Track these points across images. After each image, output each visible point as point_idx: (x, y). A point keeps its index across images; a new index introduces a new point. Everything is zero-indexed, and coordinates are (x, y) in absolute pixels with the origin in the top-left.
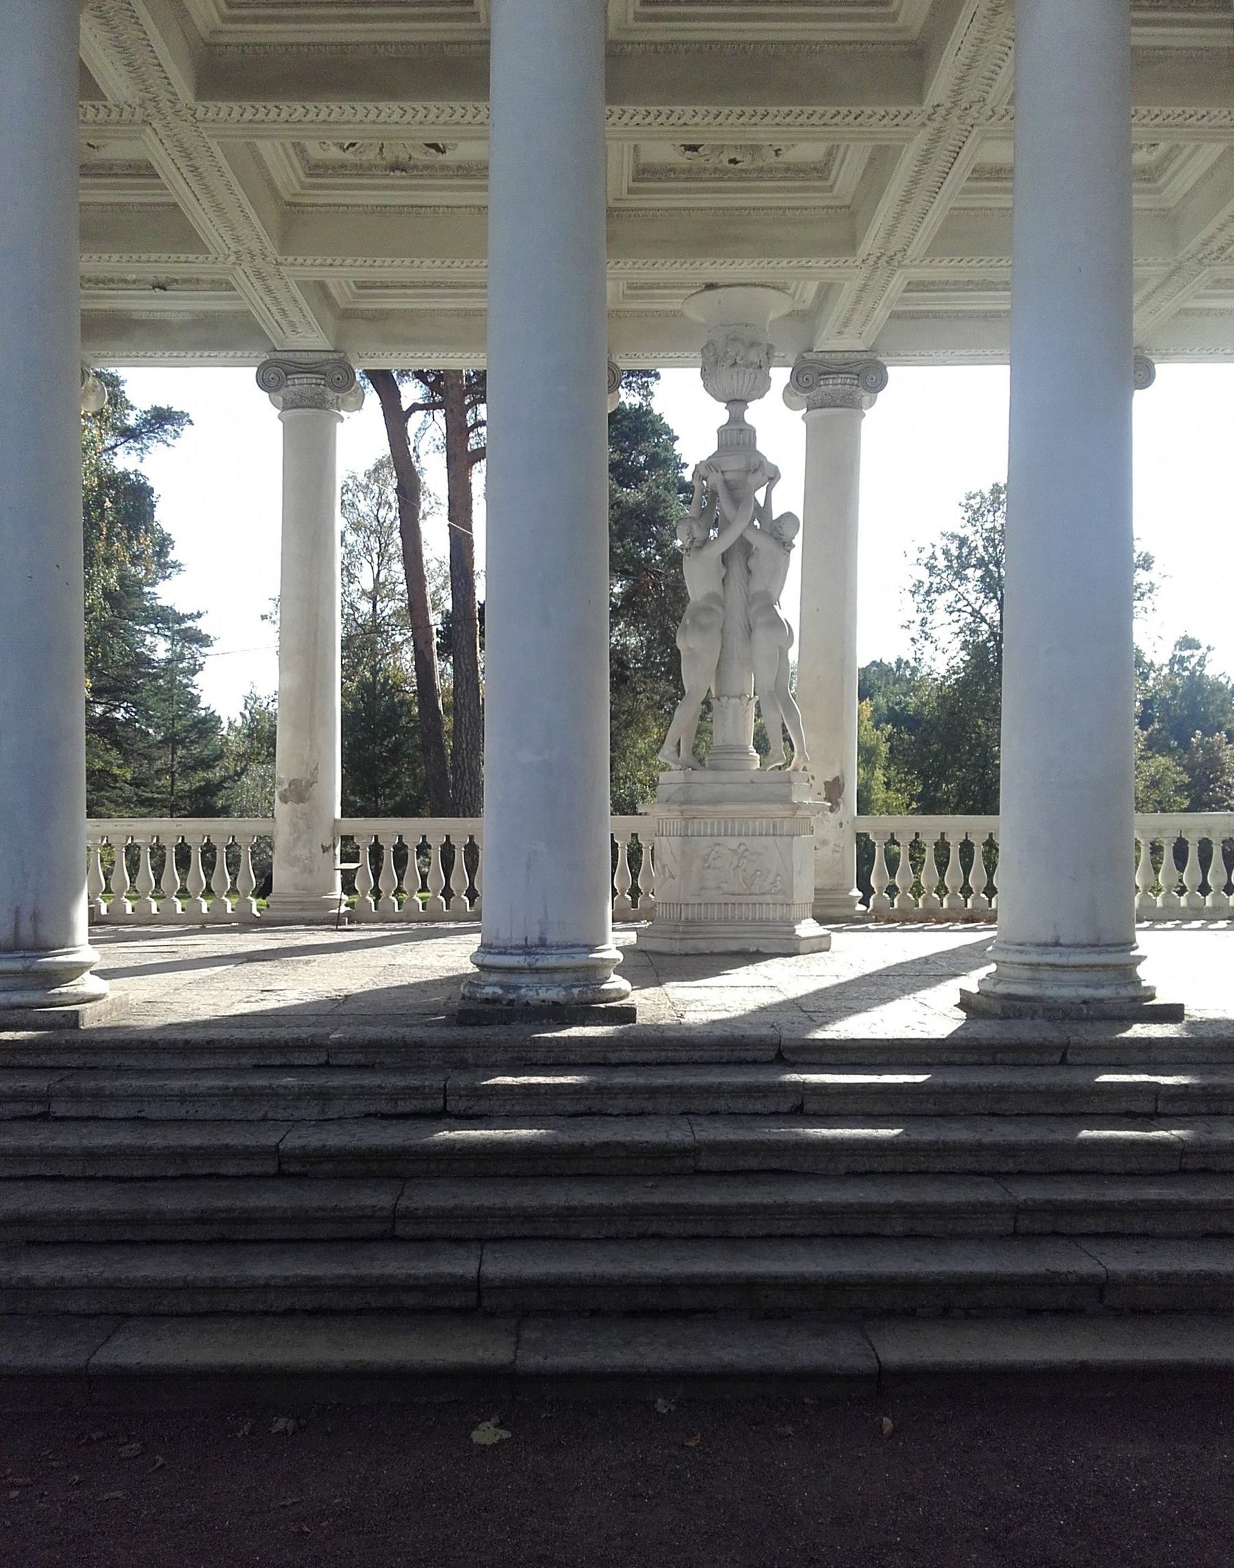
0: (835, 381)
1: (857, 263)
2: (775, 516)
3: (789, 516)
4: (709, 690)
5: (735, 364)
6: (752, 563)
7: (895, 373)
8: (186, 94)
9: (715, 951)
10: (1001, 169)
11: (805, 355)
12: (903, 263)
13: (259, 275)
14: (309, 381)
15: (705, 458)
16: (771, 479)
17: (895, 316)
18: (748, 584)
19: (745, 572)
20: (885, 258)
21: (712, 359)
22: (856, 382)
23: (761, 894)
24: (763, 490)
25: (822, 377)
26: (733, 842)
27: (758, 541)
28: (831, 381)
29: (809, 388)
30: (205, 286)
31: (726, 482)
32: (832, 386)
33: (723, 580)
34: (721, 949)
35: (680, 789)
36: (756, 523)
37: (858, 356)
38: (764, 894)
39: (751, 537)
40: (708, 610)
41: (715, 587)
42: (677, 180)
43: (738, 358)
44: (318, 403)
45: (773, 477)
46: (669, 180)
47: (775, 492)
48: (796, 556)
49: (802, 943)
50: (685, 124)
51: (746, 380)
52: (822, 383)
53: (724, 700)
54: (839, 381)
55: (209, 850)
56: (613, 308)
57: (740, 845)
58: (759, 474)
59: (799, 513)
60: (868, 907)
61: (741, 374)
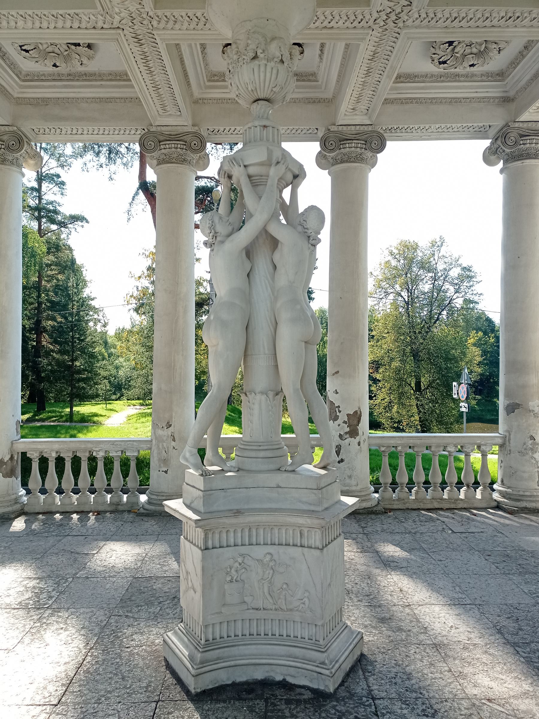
0: (350, 145)
2: (301, 210)
3: (313, 209)
5: (255, 57)
7: (389, 144)
11: (330, 127)
16: (295, 177)
19: (271, 268)
22: (364, 146)
23: (288, 610)
25: (342, 143)
26: (259, 552)
28: (347, 145)
32: (349, 149)
37: (366, 128)
38: (291, 610)
39: (273, 230)
43: (259, 51)
44: (359, 159)
47: (301, 190)
51: (268, 75)
52: (341, 146)
61: (262, 69)
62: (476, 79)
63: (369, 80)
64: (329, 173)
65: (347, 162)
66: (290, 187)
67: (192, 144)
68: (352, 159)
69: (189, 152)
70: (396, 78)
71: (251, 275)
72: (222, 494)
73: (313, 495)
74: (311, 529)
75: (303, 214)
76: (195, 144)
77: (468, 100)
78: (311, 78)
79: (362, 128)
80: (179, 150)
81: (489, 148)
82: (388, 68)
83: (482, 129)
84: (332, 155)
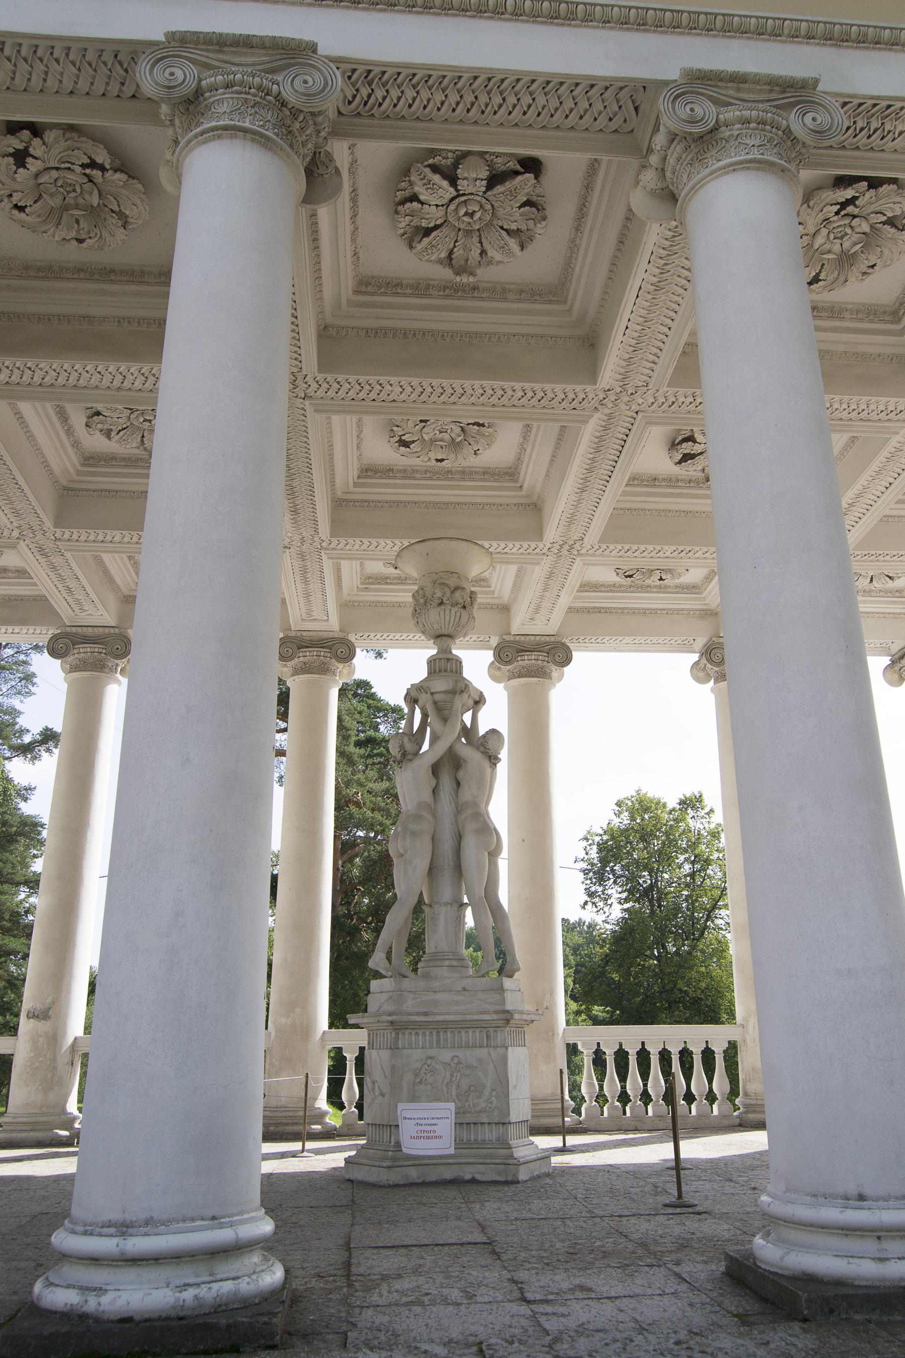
0: (530, 657)
1: (544, 551)
3: (493, 732)
4: (421, 894)
5: (441, 603)
6: (461, 774)
8: (48, 524)
9: (427, 1180)
10: (655, 479)
12: (582, 552)
13: (41, 549)
14: (92, 650)
15: (417, 682)
17: (570, 610)
18: (457, 796)
20: (566, 547)
21: (422, 601)
22: (547, 659)
24: (470, 713)
27: (466, 751)
28: (526, 657)
29: (508, 663)
30: (11, 575)
31: (435, 703)
32: (527, 660)
33: (433, 791)
34: (434, 1178)
35: (390, 998)
36: (463, 740)
37: (547, 639)
40: (418, 817)
41: (427, 796)
42: (394, 478)
43: (445, 599)
45: (479, 701)
46: (389, 478)
48: (502, 769)
49: (522, 1168)
50: (394, 400)
52: (519, 658)
53: (436, 907)
54: (533, 657)
55: (643, 1056)
56: (349, 599)
57: (452, 1058)
58: (465, 696)
59: (504, 729)
60: (580, 1116)
61: (448, 612)
62: (670, 590)
63: (547, 594)
64: (505, 688)
65: (526, 676)
66: (471, 712)
67: (339, 652)
68: (533, 673)
69: (333, 660)
70: (629, 481)
71: (436, 790)
72: (411, 995)
73: (498, 995)
74: (496, 1029)
75: (484, 736)
76: (342, 652)
77: (665, 612)
78: (482, 583)
79: (543, 639)
80: (321, 658)
81: (696, 664)
82: (567, 585)
83: (686, 642)
84: (508, 667)
